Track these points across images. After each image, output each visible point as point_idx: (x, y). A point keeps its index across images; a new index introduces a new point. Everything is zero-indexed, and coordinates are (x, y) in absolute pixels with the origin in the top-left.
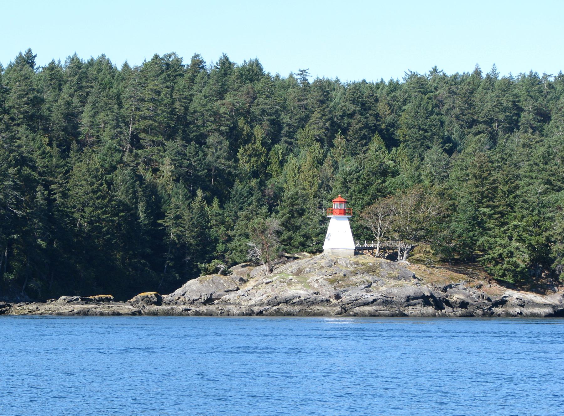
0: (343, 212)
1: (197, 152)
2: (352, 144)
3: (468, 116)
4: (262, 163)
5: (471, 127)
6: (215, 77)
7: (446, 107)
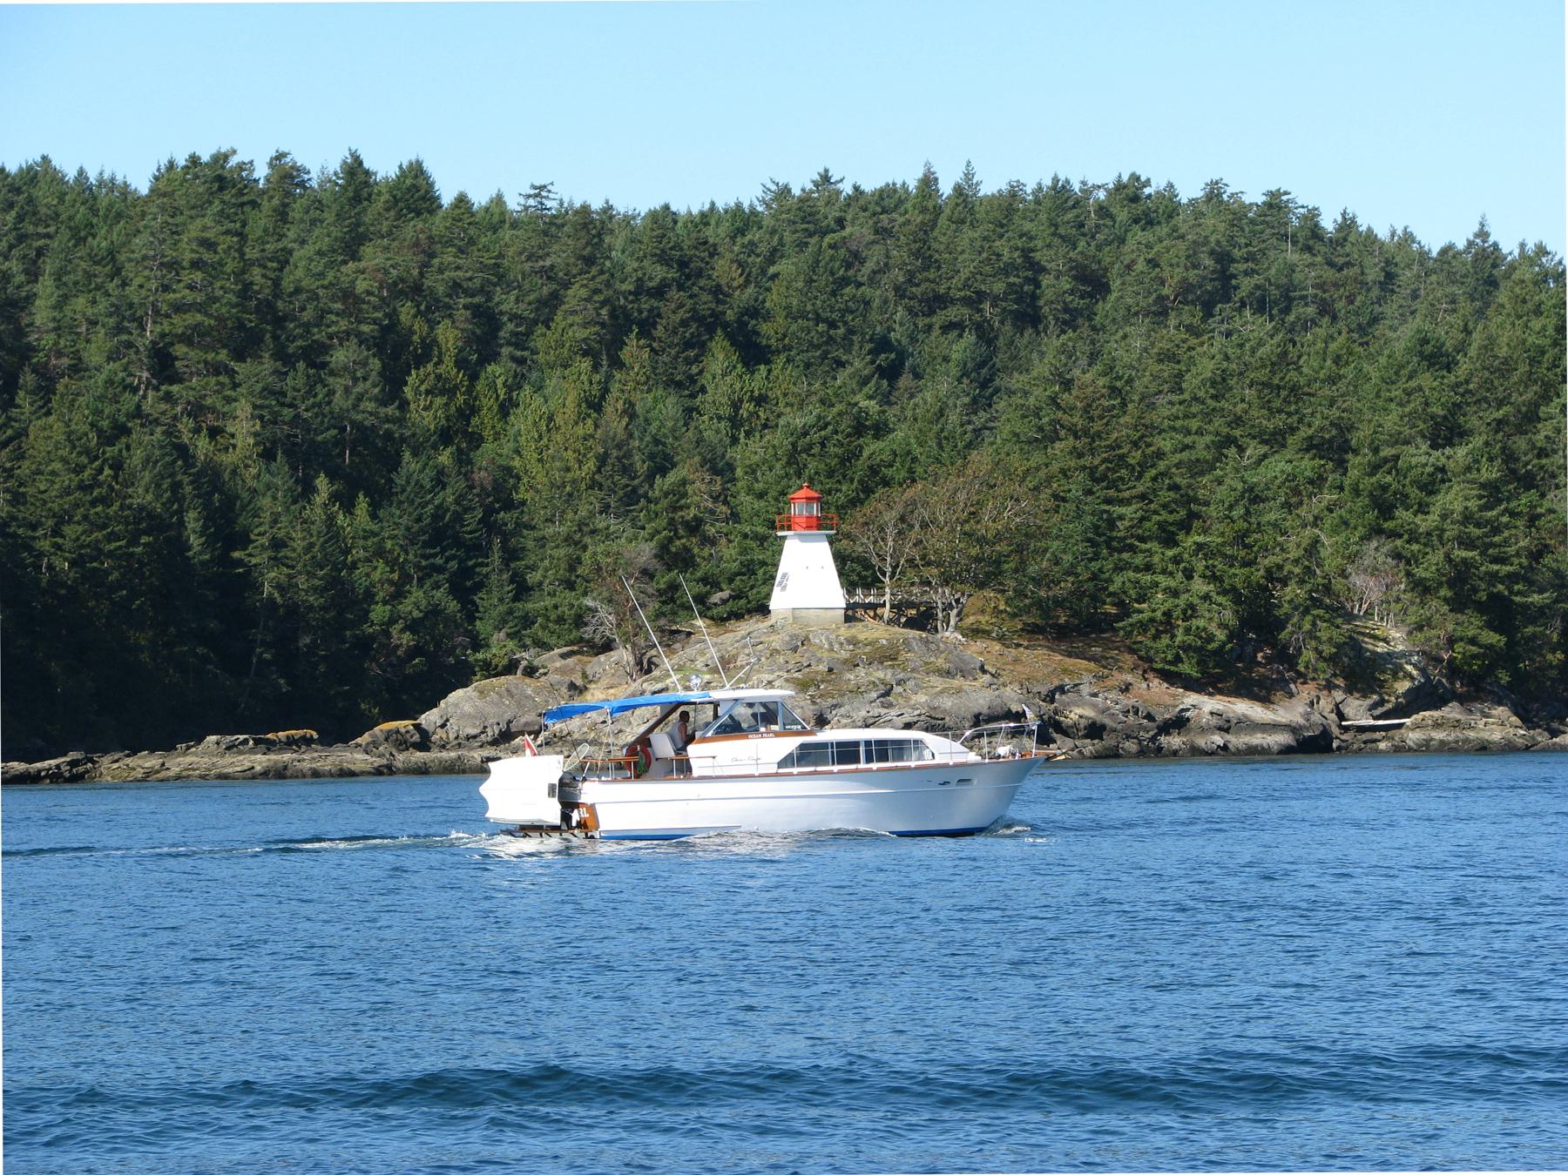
0: (814, 522)
1: (312, 387)
2: (665, 358)
3: (924, 286)
4: (459, 410)
5: (931, 313)
6: (335, 207)
7: (870, 265)
